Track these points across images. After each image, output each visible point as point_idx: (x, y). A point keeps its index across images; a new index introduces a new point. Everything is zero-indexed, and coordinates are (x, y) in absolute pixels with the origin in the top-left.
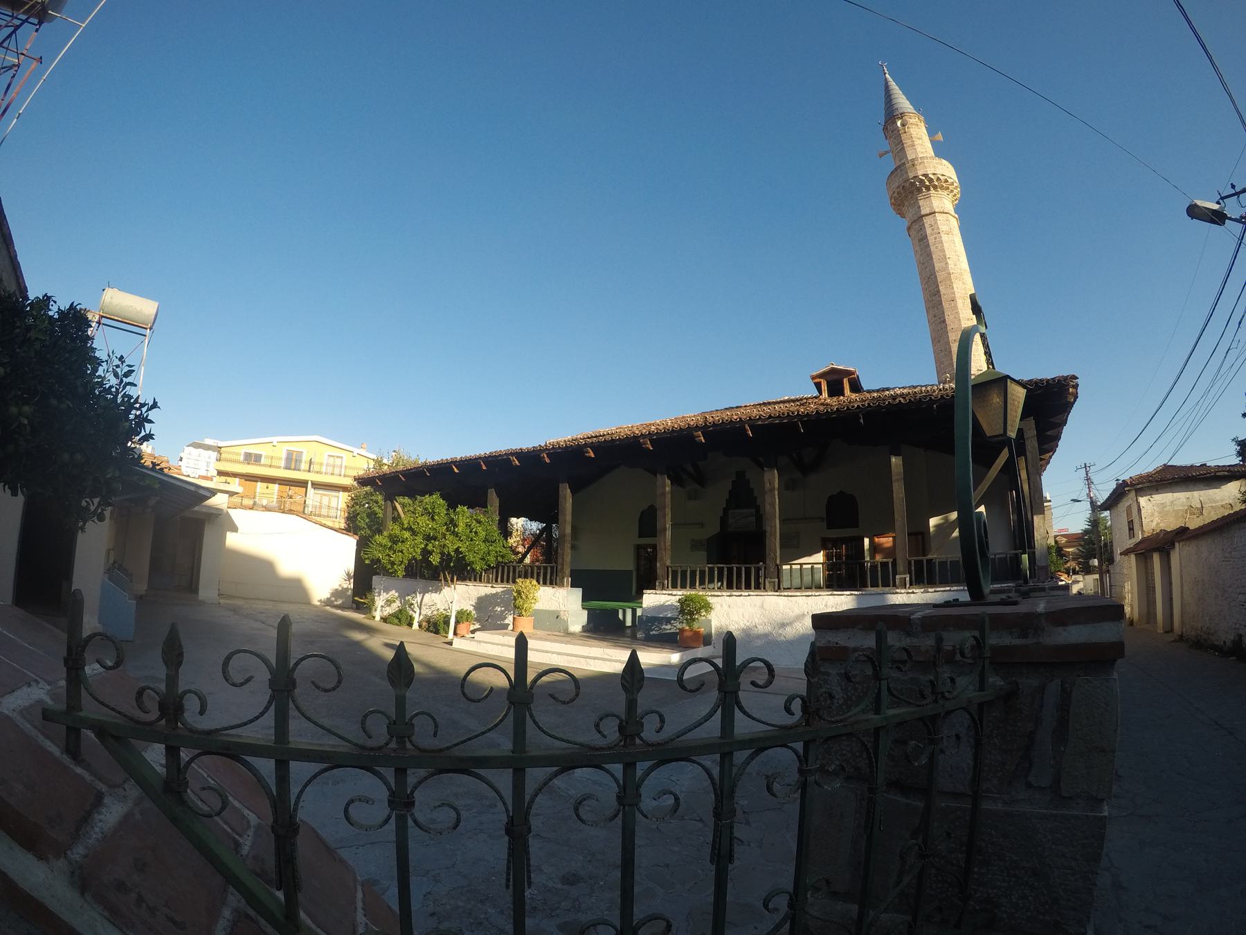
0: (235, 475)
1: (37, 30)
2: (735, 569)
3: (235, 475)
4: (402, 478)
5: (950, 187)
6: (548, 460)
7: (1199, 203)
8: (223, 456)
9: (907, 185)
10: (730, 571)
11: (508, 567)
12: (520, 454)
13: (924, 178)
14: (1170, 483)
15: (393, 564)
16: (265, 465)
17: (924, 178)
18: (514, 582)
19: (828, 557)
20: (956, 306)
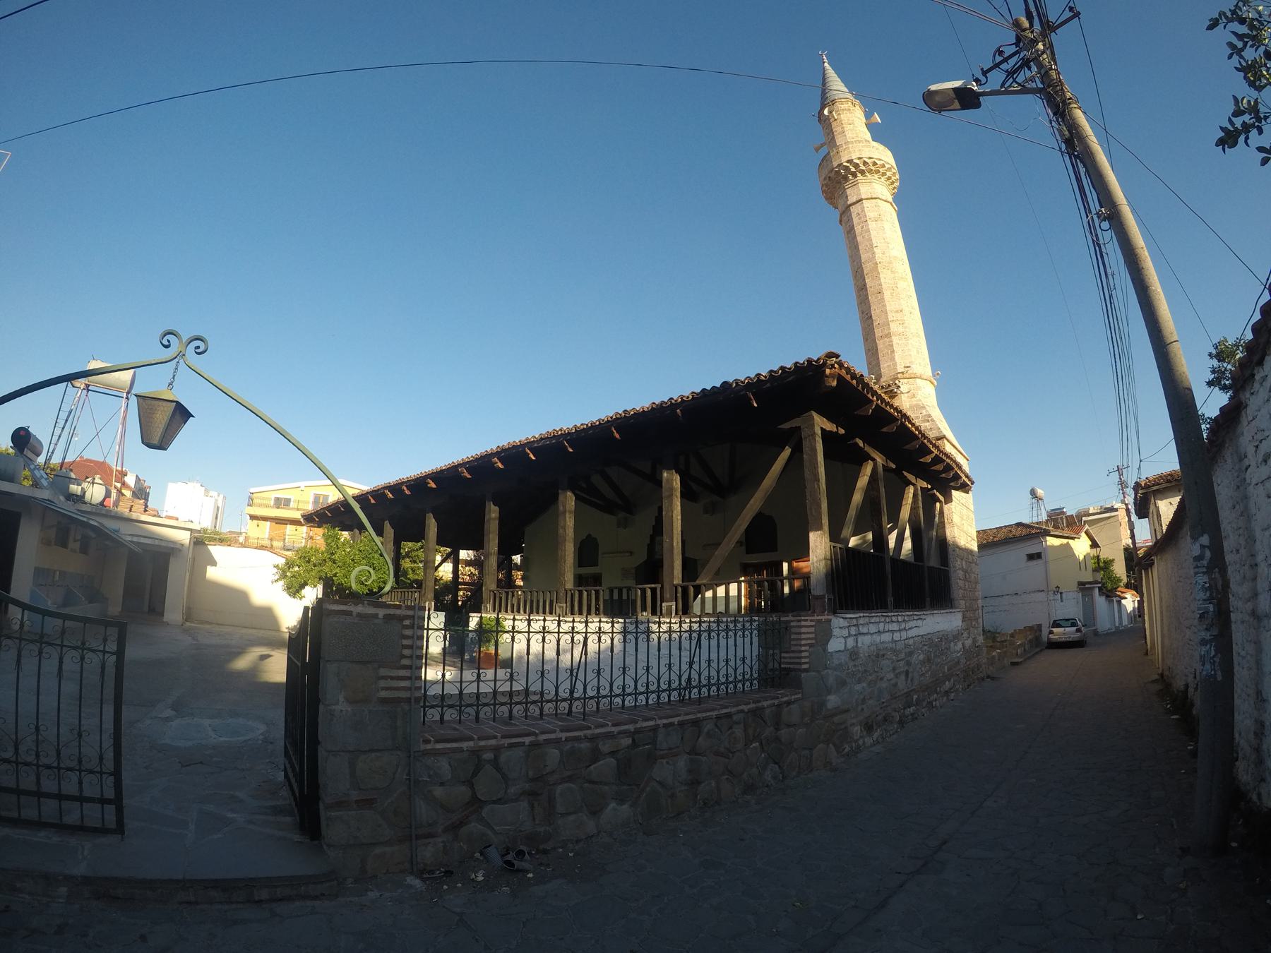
0: (265, 519)
3: (265, 519)
4: (328, 514)
5: (881, 170)
7: (933, 88)
8: (255, 501)
9: (832, 175)
13: (849, 165)
16: (293, 509)
17: (849, 165)
20: (883, 299)
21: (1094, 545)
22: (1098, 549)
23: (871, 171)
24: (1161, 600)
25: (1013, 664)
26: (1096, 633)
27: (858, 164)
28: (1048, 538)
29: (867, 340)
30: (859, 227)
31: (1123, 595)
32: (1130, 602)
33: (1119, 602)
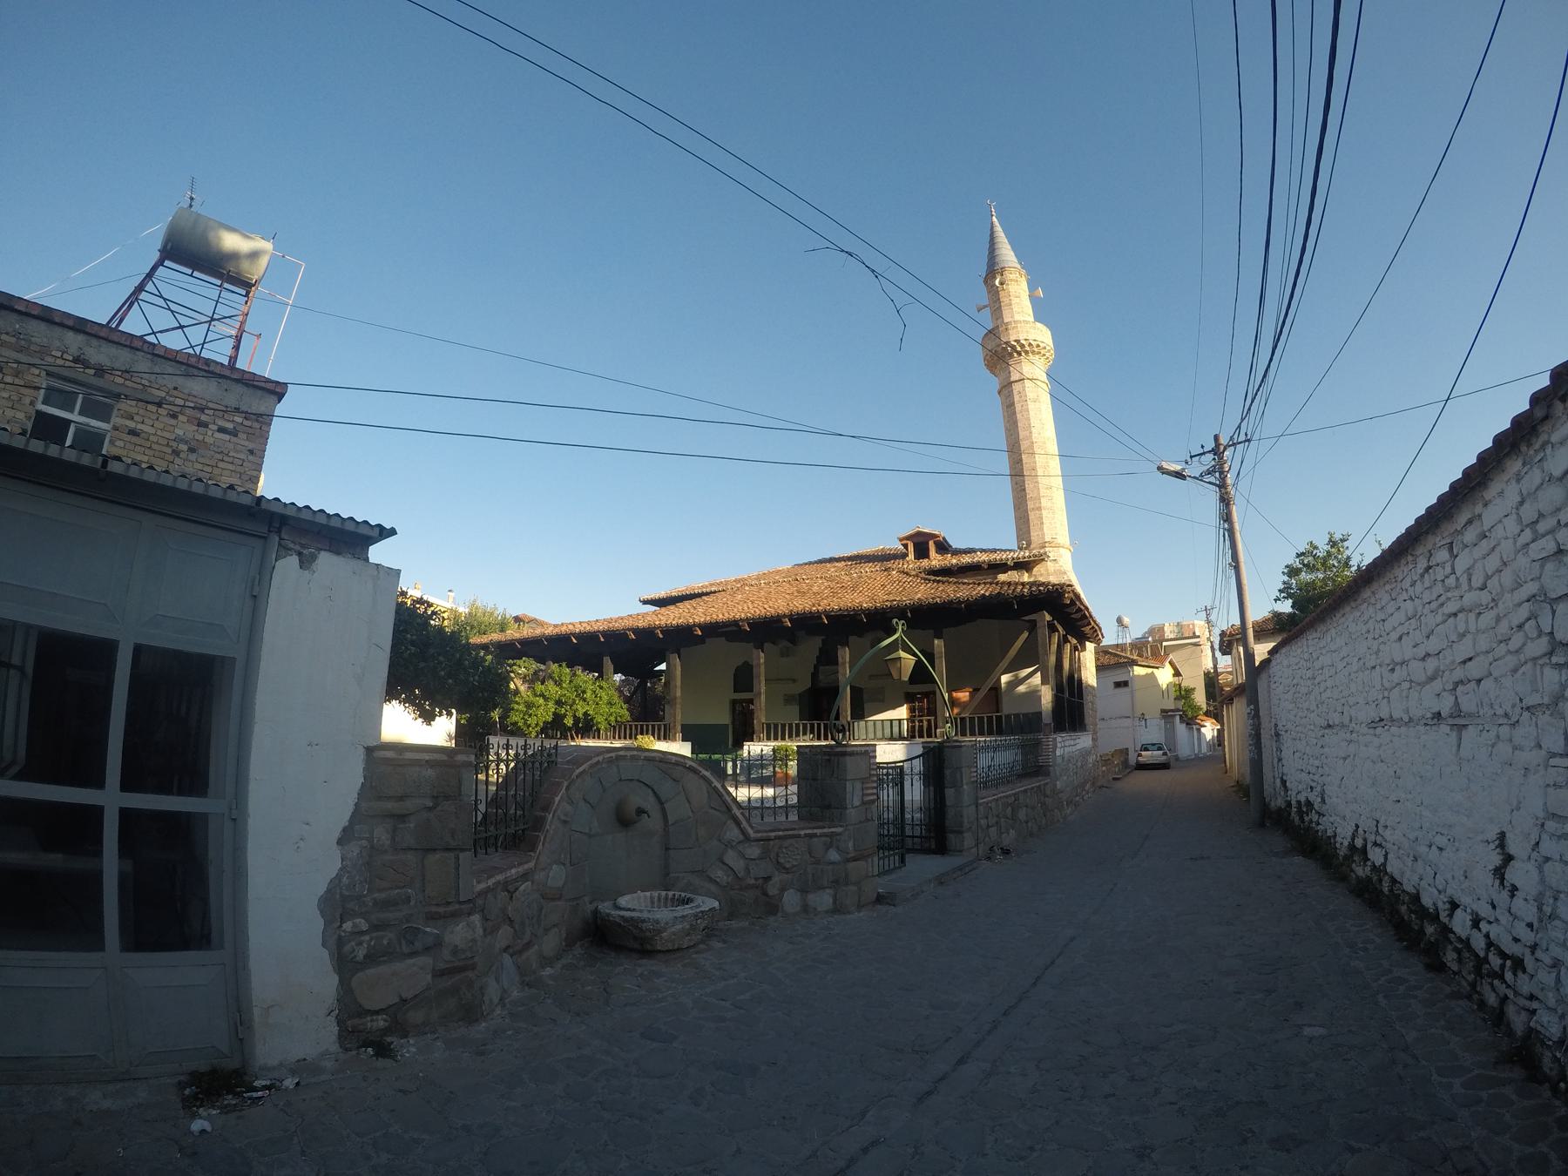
1: (246, 303)
2: (816, 725)
6: (661, 636)
9: (999, 349)
11: (625, 726)
12: (636, 631)
13: (1016, 344)
14: (1272, 633)
15: (529, 726)
17: (1016, 344)
18: (636, 739)
19: (912, 710)
21: (1177, 674)
22: (1181, 678)
23: (1033, 352)
24: (1237, 729)
25: (1114, 779)
26: (1177, 758)
27: (1023, 345)
28: (1135, 668)
29: (1019, 509)
30: (1020, 405)
32: (1209, 730)
33: (1199, 730)
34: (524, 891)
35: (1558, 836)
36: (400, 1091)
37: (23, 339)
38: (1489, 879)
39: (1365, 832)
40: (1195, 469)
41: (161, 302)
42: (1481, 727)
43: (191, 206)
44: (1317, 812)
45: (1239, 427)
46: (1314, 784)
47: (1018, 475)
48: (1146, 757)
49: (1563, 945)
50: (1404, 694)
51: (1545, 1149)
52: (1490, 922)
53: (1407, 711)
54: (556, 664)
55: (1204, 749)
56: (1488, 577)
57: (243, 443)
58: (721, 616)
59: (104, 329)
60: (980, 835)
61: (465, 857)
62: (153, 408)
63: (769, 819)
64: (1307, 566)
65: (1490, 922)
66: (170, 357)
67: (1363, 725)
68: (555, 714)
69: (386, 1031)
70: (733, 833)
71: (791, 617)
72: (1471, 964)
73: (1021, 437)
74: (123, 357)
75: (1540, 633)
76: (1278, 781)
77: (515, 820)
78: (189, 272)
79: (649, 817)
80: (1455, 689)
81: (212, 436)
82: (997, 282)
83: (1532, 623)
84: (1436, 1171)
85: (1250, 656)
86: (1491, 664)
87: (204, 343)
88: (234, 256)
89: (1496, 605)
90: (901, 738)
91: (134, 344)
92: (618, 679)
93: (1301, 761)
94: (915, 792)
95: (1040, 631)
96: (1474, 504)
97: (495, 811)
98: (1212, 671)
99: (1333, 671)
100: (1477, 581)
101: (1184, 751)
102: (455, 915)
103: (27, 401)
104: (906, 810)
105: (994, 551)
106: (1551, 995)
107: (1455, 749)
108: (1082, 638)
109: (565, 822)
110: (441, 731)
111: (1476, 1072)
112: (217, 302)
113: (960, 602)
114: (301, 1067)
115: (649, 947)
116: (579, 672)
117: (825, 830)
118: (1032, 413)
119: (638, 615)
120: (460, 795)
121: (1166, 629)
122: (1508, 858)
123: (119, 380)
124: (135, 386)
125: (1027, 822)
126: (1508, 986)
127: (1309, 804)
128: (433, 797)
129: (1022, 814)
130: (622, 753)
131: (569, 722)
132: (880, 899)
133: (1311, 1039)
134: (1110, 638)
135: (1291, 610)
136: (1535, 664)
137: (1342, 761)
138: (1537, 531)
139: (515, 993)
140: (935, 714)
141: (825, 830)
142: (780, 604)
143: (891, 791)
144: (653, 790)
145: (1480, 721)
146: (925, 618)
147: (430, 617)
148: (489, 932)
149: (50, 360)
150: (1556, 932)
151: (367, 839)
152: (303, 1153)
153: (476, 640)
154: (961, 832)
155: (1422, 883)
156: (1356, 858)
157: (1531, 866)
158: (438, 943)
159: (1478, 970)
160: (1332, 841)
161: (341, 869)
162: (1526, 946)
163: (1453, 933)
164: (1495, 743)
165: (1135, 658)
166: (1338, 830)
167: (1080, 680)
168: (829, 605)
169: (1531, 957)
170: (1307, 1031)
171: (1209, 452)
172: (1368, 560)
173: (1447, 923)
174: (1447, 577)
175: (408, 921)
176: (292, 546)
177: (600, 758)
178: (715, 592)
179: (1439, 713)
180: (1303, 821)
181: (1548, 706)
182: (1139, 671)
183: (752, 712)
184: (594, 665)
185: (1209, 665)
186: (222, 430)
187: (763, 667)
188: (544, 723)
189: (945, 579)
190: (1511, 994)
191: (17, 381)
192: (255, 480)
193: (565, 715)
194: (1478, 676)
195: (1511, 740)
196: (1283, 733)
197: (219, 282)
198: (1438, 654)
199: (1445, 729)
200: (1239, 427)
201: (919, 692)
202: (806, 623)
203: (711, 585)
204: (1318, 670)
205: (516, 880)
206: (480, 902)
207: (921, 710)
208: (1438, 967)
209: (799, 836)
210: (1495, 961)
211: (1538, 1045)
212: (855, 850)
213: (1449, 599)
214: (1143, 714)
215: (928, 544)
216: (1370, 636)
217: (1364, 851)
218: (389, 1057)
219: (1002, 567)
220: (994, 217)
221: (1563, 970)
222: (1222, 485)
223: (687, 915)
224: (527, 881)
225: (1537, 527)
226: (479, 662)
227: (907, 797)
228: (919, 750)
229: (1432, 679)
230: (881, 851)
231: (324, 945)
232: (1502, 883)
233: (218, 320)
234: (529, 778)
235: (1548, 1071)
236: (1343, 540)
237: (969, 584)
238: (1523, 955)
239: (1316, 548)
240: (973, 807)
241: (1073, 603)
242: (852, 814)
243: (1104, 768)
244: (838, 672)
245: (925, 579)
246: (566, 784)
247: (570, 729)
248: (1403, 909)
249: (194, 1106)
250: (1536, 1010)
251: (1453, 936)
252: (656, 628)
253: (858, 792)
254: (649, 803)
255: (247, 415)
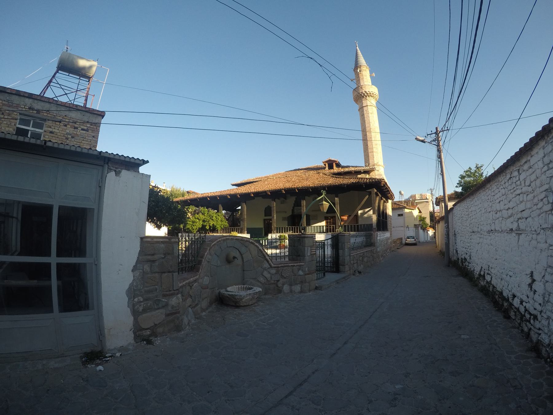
1: (89, 84)
6: (239, 197)
9: (359, 95)
10: (292, 228)
12: (230, 195)
13: (365, 93)
15: (193, 229)
17: (365, 93)
18: (231, 233)
19: (327, 223)
21: (420, 212)
22: (421, 213)
23: (371, 96)
25: (397, 248)
26: (419, 242)
28: (405, 209)
30: (366, 115)
31: (428, 230)
32: (431, 232)
33: (427, 232)
34: (195, 286)
35: (551, 274)
36: (156, 355)
37: (10, 102)
38: (527, 287)
39: (484, 269)
40: (429, 139)
41: (58, 86)
42: (526, 235)
43: (67, 51)
44: (468, 262)
45: (445, 125)
46: (467, 252)
47: (365, 140)
48: (409, 241)
49: (551, 311)
50: (500, 222)
51: (542, 381)
52: (526, 303)
53: (501, 228)
54: (203, 208)
55: (429, 239)
56: (531, 182)
57: (90, 134)
58: (260, 190)
59: (39, 97)
60: (351, 266)
61: (176, 274)
62: (58, 123)
63: (278, 260)
64: (468, 175)
65: (526, 303)
66: (63, 105)
67: (485, 232)
68: (202, 225)
69: (150, 335)
70: (266, 265)
71: (285, 190)
72: (519, 317)
73: (366, 126)
74: (47, 106)
75: (549, 203)
76: (455, 251)
77: (192, 261)
78: (68, 74)
79: (237, 259)
80: (518, 221)
81: (79, 132)
82: (358, 71)
83: (546, 199)
84: (505, 386)
85: (446, 206)
86: (531, 213)
87: (75, 99)
88: (84, 68)
89: (534, 192)
90: (323, 232)
91: (50, 101)
92: (224, 212)
93: (463, 244)
94: (329, 251)
95: (372, 195)
96: (527, 156)
97: (185, 258)
98: (432, 211)
99: (475, 213)
100: (527, 183)
101: (422, 239)
102: (172, 295)
103: (13, 124)
104: (326, 257)
105: (357, 167)
106: (546, 328)
107: (517, 241)
108: (387, 198)
109: (208, 262)
110: (163, 231)
111: (519, 353)
112: (78, 84)
113: (344, 185)
114: (121, 349)
115: (238, 305)
116: (210, 210)
117: (298, 264)
118: (370, 118)
119: (231, 189)
120: (173, 253)
121: (416, 196)
122: (534, 281)
123: (45, 114)
124: (51, 116)
125: (367, 262)
126: (532, 325)
127: (465, 259)
128: (164, 254)
129: (365, 259)
130: (228, 237)
131: (208, 228)
132: (317, 288)
133: (464, 339)
134: (397, 198)
135: (461, 191)
136: (546, 214)
137: (477, 244)
138: (549, 166)
139: (193, 321)
140: (335, 224)
141: (298, 264)
142: (281, 185)
143: (320, 250)
144: (239, 250)
145: (526, 232)
146: (332, 190)
147: (159, 192)
148: (184, 300)
149: (20, 109)
150: (549, 307)
151: (142, 269)
152: (124, 378)
153: (175, 200)
154: (344, 265)
155: (504, 288)
156: (481, 278)
157: (541, 284)
158: (167, 305)
159: (521, 319)
160: (473, 272)
161: (133, 280)
162: (538, 311)
163: (514, 306)
164: (531, 240)
165: (406, 206)
166: (475, 269)
167: (386, 213)
168: (298, 185)
169: (540, 315)
170: (463, 336)
171: (434, 133)
172: (489, 174)
173: (512, 302)
174: (517, 181)
175: (156, 297)
176: (112, 168)
177: (220, 239)
178: (258, 181)
179: (512, 229)
180: (463, 264)
181: (550, 228)
182: (407, 210)
183: (271, 224)
184: (215, 207)
185: (431, 209)
186: (83, 130)
187: (275, 207)
188: (199, 228)
189: (339, 176)
190: (533, 328)
191: (9, 117)
192: (96, 146)
193: (206, 225)
194: (526, 217)
195: (536, 239)
196: (457, 234)
197: (78, 77)
198: (513, 208)
199: (514, 234)
200: (445, 125)
201: (330, 216)
202: (290, 192)
203: (256, 179)
204: (470, 212)
205: (192, 282)
206: (181, 290)
207: (330, 223)
208: (508, 317)
209: (289, 266)
210: (528, 316)
211: (541, 346)
212: (308, 271)
213: (517, 189)
214: (408, 226)
215: (333, 164)
216: (489, 201)
217: (484, 276)
218: (151, 344)
219: (359, 172)
220: (357, 47)
221: (551, 320)
222: (438, 145)
223: (251, 293)
224: (196, 282)
225: (549, 166)
226: (176, 208)
227: (326, 253)
228: (330, 236)
229: (510, 217)
230: (317, 272)
231: (128, 307)
232: (531, 289)
233: (79, 91)
234: (196, 247)
235: (544, 355)
236: (481, 167)
237: (348, 178)
238: (537, 314)
239: (471, 169)
240: (349, 257)
241: (384, 186)
242: (307, 258)
243: (394, 244)
244: (301, 209)
245: (332, 177)
246: (209, 248)
247: (208, 230)
248: (497, 297)
249: (86, 364)
250: (541, 334)
251: (514, 307)
252: (237, 194)
253: (309, 251)
254: (237, 254)
255: (92, 124)
